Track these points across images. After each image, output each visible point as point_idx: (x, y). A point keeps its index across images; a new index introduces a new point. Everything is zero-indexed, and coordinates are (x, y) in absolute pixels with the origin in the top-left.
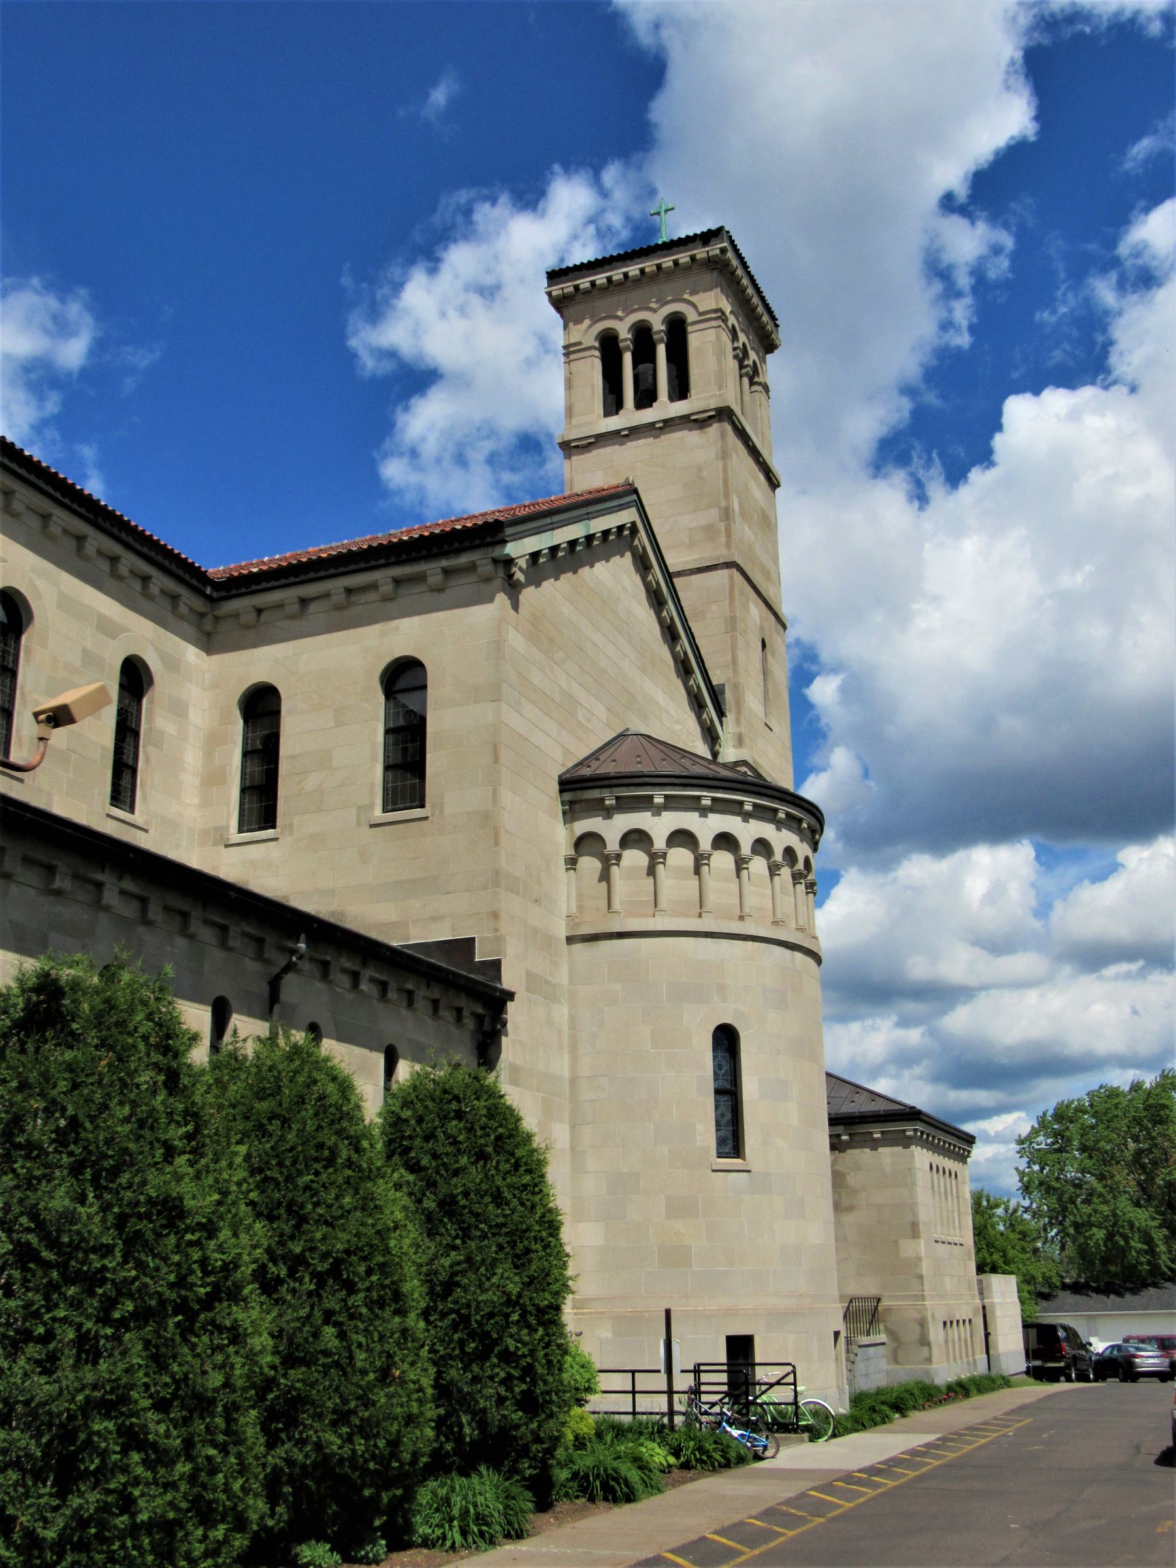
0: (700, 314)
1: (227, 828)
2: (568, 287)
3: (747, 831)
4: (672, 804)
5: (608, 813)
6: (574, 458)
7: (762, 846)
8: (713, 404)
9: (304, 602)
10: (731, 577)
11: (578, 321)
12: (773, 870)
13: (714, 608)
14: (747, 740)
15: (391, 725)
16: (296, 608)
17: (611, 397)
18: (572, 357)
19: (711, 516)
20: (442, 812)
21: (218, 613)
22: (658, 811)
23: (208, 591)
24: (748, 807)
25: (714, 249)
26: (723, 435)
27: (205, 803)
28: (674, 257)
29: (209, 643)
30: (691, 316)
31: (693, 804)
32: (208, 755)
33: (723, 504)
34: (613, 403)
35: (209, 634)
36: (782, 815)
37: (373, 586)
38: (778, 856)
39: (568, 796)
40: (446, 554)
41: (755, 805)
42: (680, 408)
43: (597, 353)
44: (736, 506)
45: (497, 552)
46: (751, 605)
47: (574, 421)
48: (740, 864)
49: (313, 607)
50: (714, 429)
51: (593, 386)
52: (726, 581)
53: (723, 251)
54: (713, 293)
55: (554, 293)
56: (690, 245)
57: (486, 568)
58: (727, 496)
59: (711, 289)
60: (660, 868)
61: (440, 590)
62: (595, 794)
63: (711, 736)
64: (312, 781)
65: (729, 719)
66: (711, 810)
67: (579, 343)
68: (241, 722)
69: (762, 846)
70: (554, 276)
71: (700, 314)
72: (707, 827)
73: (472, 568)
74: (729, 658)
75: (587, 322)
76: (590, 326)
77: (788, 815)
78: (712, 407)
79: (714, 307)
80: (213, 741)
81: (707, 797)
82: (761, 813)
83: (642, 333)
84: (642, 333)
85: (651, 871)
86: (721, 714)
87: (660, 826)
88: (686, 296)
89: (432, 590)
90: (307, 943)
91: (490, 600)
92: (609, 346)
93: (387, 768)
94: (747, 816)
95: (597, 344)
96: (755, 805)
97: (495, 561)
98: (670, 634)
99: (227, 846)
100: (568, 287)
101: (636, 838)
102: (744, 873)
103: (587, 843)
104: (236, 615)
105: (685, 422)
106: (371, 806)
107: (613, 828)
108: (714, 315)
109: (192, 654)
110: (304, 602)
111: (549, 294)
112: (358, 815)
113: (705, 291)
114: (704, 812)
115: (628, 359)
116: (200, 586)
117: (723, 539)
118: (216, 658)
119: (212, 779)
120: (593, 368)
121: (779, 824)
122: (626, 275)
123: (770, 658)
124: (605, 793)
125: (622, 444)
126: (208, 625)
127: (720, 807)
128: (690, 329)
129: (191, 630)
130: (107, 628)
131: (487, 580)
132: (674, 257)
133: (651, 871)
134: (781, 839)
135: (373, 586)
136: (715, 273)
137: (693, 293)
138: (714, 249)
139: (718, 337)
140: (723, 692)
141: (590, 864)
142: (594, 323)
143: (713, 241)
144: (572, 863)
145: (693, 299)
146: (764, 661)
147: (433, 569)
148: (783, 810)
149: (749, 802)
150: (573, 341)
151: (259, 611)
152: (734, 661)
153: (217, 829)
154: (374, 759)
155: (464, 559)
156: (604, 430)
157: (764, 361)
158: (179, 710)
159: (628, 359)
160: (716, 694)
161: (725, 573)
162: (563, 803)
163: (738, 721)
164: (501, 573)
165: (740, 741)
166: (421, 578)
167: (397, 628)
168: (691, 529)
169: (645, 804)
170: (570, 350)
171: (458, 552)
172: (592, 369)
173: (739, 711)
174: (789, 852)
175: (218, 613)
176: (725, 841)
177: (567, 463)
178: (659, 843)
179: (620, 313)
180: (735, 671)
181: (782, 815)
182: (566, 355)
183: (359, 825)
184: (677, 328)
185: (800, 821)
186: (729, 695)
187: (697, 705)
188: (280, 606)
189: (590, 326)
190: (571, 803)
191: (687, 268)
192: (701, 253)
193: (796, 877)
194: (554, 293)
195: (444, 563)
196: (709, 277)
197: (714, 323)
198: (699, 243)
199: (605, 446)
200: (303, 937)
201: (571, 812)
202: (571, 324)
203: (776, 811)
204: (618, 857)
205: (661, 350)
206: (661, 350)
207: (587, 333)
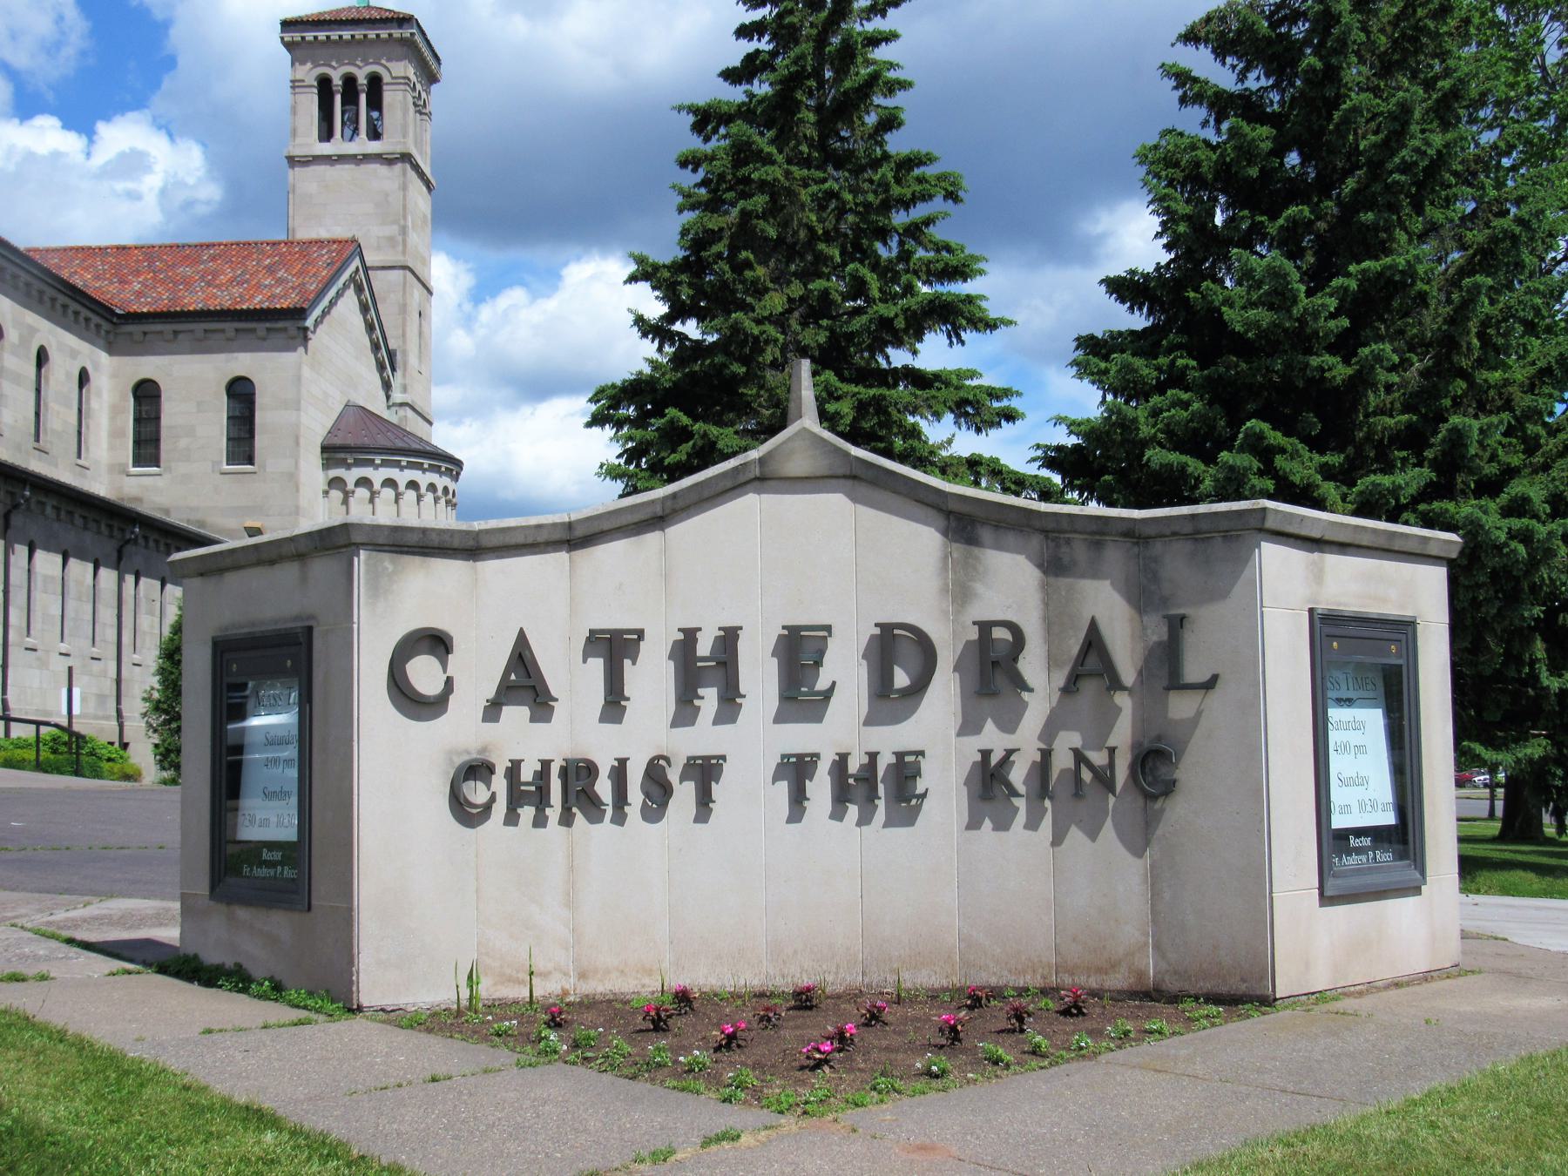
0: (393, 78)
1: (127, 465)
2: (297, 36)
3: (424, 479)
4: (385, 464)
5: (349, 467)
6: (296, 169)
7: (432, 487)
8: (399, 149)
9: (176, 333)
10: (405, 277)
11: (303, 63)
12: (436, 500)
13: (392, 296)
14: (409, 387)
15: (231, 414)
16: (172, 336)
17: (325, 125)
18: (297, 90)
19: (393, 230)
20: (265, 471)
21: (118, 331)
22: (377, 467)
23: (115, 320)
24: (426, 466)
25: (406, 33)
26: (404, 174)
27: (111, 448)
28: (377, 32)
29: (111, 350)
30: (386, 78)
31: (397, 464)
32: (113, 418)
33: (402, 222)
34: (326, 134)
35: (110, 343)
36: (443, 469)
37: (223, 331)
38: (440, 493)
39: (325, 456)
40: (267, 320)
41: (430, 465)
42: (374, 147)
43: (316, 91)
44: (410, 224)
45: (300, 324)
46: (415, 291)
47: (298, 140)
48: (419, 498)
49: (181, 336)
50: (398, 167)
51: (312, 116)
52: (402, 278)
53: (412, 34)
54: (403, 63)
55: (286, 39)
56: (389, 25)
57: (293, 331)
58: (405, 218)
59: (401, 60)
60: (377, 500)
61: (264, 339)
62: (342, 455)
63: (387, 386)
64: (183, 443)
65: (399, 373)
66: (406, 467)
67: (303, 81)
68: (132, 400)
69: (432, 487)
70: (287, 25)
71: (393, 78)
72: (403, 477)
73: (285, 330)
74: (401, 332)
75: (309, 65)
76: (312, 69)
77: (446, 468)
78: (399, 151)
79: (402, 74)
80: (115, 411)
81: (404, 460)
82: (433, 469)
83: (350, 81)
84: (350, 81)
85: (372, 501)
86: (393, 369)
87: (377, 476)
88: (383, 62)
89: (259, 338)
90: (140, 528)
91: (295, 350)
92: (324, 84)
93: (229, 439)
94: (424, 471)
95: (316, 84)
96: (430, 465)
97: (299, 328)
98: (370, 328)
99: (128, 475)
100: (297, 36)
101: (364, 482)
102: (422, 503)
103: (337, 483)
104: (130, 334)
105: (378, 158)
106: (221, 462)
107: (351, 476)
108: (402, 81)
109: (103, 357)
110: (176, 333)
111: (282, 38)
112: (213, 466)
113: (397, 61)
114: (402, 468)
115: (338, 99)
116: (109, 317)
117: (400, 248)
118: (116, 359)
119: (116, 434)
120: (312, 102)
121: (441, 474)
122: (340, 37)
123: (423, 322)
124: (348, 456)
125: (332, 165)
126: (111, 337)
127: (411, 466)
128: (385, 87)
129: (102, 342)
130: (74, 354)
131: (293, 338)
132: (377, 32)
133: (372, 501)
134: (441, 481)
135: (223, 331)
136: (405, 48)
137: (389, 60)
138: (406, 33)
139: (405, 97)
140: (396, 355)
141: (336, 495)
142: (315, 67)
143: (406, 25)
144: (326, 493)
145: (388, 64)
146: (420, 324)
147: (261, 327)
148: (444, 466)
149: (426, 463)
150: (298, 77)
151: (145, 333)
152: (404, 335)
153: (120, 465)
154: (222, 434)
155: (280, 325)
156: (319, 153)
157: (428, 93)
158: (99, 395)
159: (338, 99)
160: (391, 355)
161: (401, 272)
162: (323, 459)
163: (404, 376)
164: (301, 335)
165: (405, 389)
166: (253, 331)
167: (236, 358)
168: (378, 238)
169: (370, 463)
170: (295, 85)
171: (277, 320)
172: (311, 102)
173: (405, 370)
174: (446, 490)
175: (118, 331)
176: (413, 485)
177: (290, 171)
178: (377, 486)
179: (334, 64)
180: (404, 342)
181: (443, 469)
182: (293, 87)
183: (213, 471)
184: (375, 82)
185: (452, 470)
186: (399, 357)
187: (381, 367)
188: (161, 332)
189: (312, 69)
190: (327, 459)
191: (386, 41)
192: (396, 33)
193: (448, 502)
194: (286, 39)
195: (268, 325)
196: (399, 50)
197: (402, 87)
198: (395, 24)
199: (320, 164)
200: (28, 487)
201: (327, 465)
202: (297, 64)
203: (440, 467)
204: (353, 492)
205: (363, 98)
206: (363, 98)
207: (309, 73)
